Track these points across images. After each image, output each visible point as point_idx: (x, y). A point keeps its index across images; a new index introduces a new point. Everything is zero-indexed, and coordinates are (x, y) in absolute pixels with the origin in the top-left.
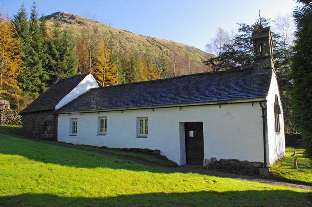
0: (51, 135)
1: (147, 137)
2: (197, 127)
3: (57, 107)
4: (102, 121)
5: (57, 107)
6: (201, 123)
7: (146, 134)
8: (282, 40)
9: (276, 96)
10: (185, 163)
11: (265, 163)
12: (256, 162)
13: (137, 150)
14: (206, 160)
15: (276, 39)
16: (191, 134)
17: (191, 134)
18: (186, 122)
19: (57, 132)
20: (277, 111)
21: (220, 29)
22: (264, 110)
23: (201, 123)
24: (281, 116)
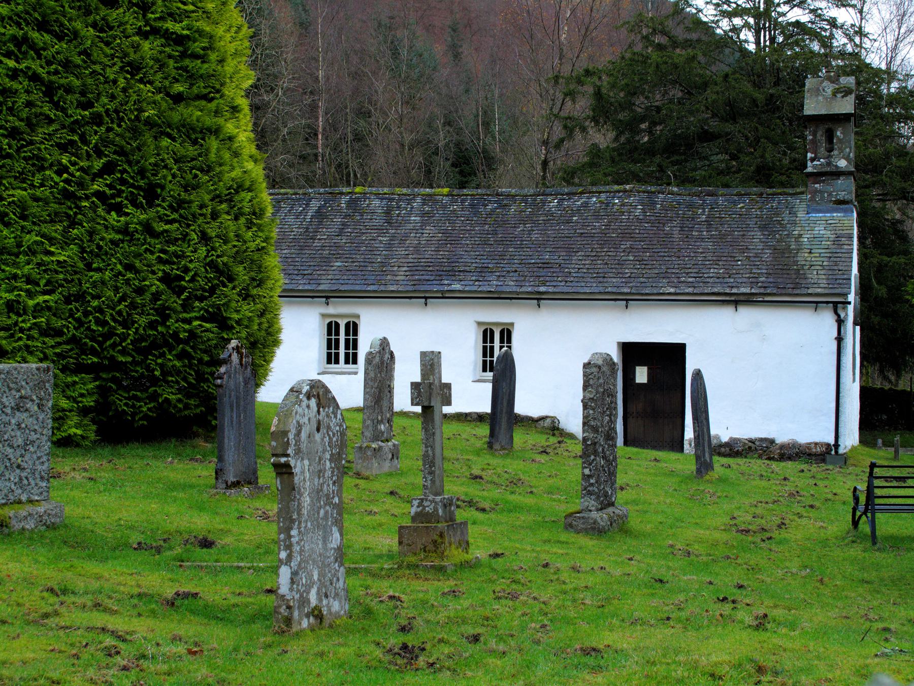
11: (837, 445)
12: (816, 444)
16: (641, 375)
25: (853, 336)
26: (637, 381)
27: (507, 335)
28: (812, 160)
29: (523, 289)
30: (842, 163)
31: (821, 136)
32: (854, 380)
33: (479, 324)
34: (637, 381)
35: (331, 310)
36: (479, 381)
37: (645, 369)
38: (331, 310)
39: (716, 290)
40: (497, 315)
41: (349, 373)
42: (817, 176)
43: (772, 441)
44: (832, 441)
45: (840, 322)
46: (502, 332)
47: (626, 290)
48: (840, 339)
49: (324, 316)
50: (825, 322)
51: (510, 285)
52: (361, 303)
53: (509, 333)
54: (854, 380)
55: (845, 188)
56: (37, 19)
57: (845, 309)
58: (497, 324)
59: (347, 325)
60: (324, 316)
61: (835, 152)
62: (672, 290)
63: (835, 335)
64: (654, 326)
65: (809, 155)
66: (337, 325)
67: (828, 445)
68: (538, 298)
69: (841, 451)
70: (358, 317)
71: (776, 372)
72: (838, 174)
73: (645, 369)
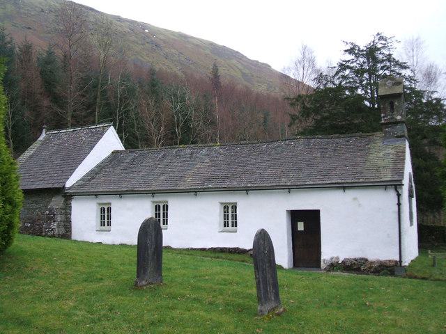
0: (62, 231)
1: (236, 232)
2: (311, 218)
3: (69, 184)
4: (102, 210)
5: (69, 184)
6: (318, 212)
7: (233, 226)
8: (412, 75)
9: (410, 174)
10: (292, 266)
11: (401, 261)
12: (390, 261)
13: (223, 250)
14: (324, 260)
15: (403, 72)
16: (301, 226)
17: (301, 226)
18: (294, 209)
19: (71, 225)
20: (411, 196)
21: (305, 48)
22: (399, 195)
23: (318, 212)
24: (414, 200)
25: (409, 206)
26: (299, 230)
27: (234, 207)
28: (384, 117)
29: (241, 186)
30: (399, 118)
31: (387, 105)
32: (411, 224)
33: (222, 204)
34: (299, 230)
35: (101, 202)
36: (223, 232)
37: (302, 223)
38: (156, 199)
39: (333, 182)
40: (229, 199)
41: (106, 231)
42: (386, 124)
43: (366, 260)
44: (398, 259)
45: (399, 195)
46: (232, 207)
47: (289, 184)
48: (399, 204)
49: (153, 202)
50: (387, 199)
51: (235, 184)
52: (134, 197)
53: (236, 207)
54: (411, 224)
55: (403, 129)
56: (437, 172)
57: (401, 188)
58: (230, 203)
59: (108, 208)
60: (153, 202)
61: (395, 113)
62: (312, 183)
63: (397, 202)
64: (304, 201)
65: (382, 115)
66: (159, 206)
67: (396, 262)
68: (247, 190)
69: (403, 264)
70: (167, 202)
71: (368, 224)
72: (397, 123)
73: (302, 223)
